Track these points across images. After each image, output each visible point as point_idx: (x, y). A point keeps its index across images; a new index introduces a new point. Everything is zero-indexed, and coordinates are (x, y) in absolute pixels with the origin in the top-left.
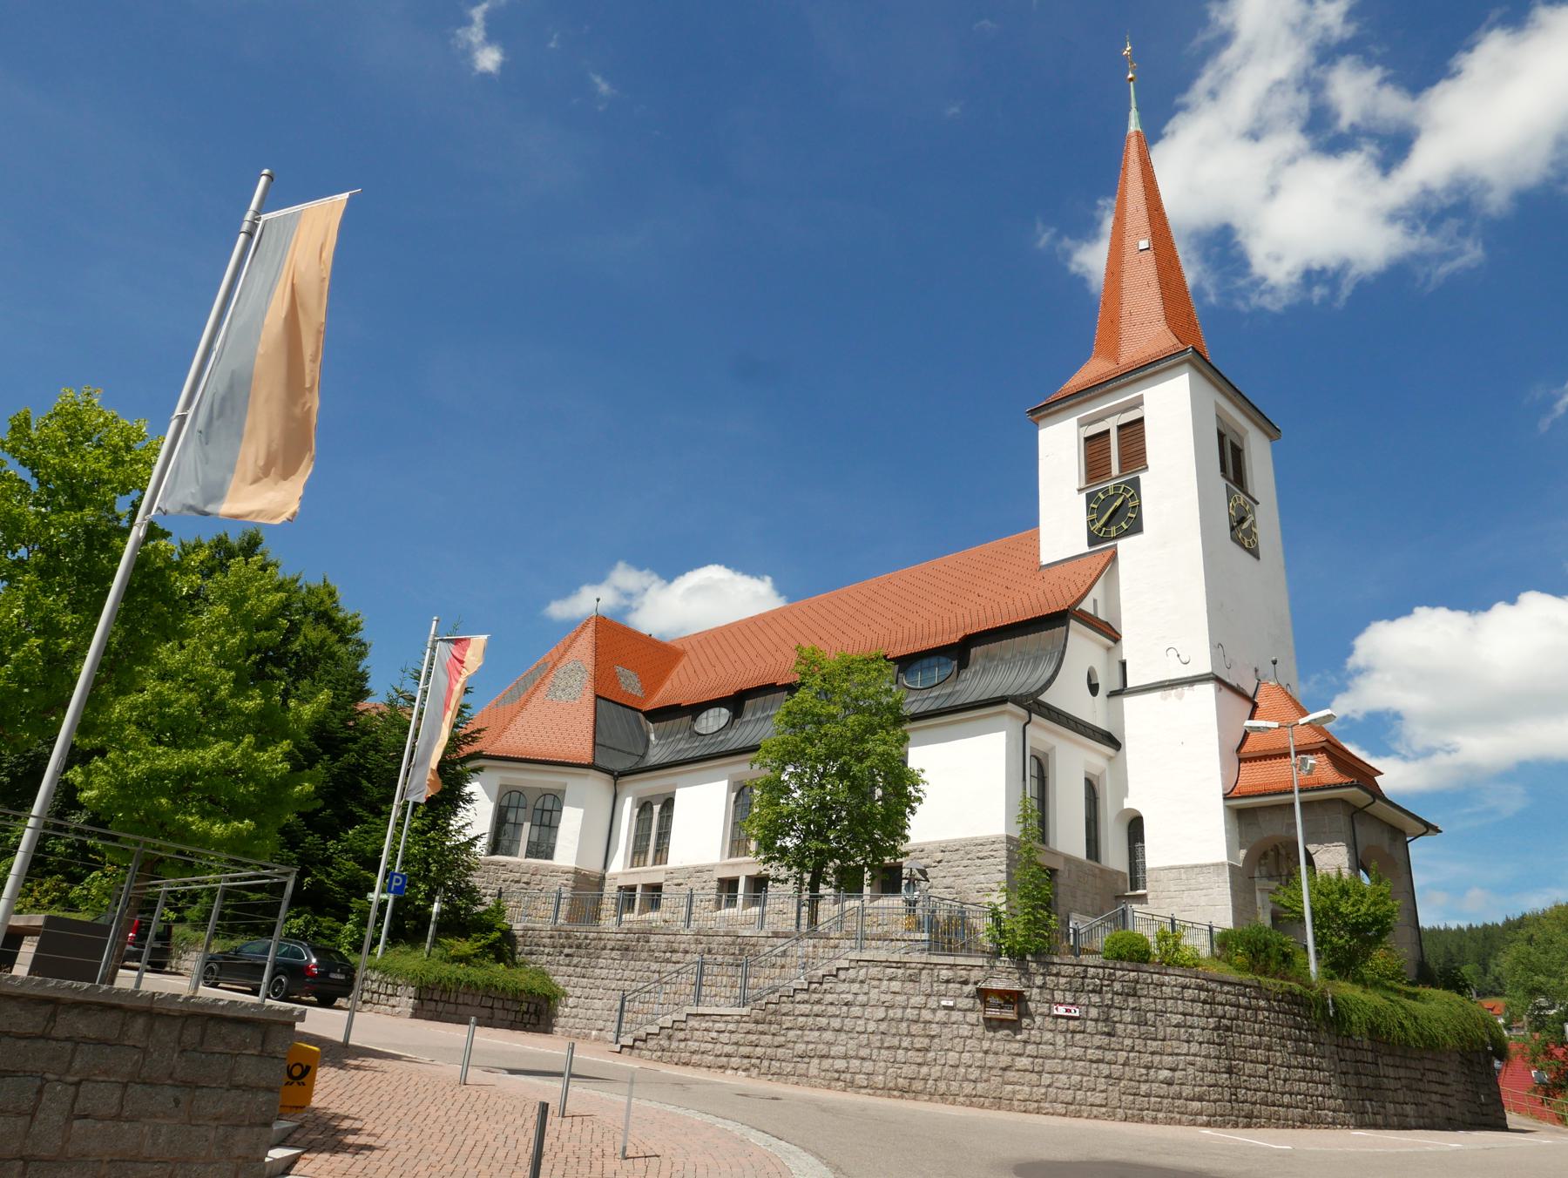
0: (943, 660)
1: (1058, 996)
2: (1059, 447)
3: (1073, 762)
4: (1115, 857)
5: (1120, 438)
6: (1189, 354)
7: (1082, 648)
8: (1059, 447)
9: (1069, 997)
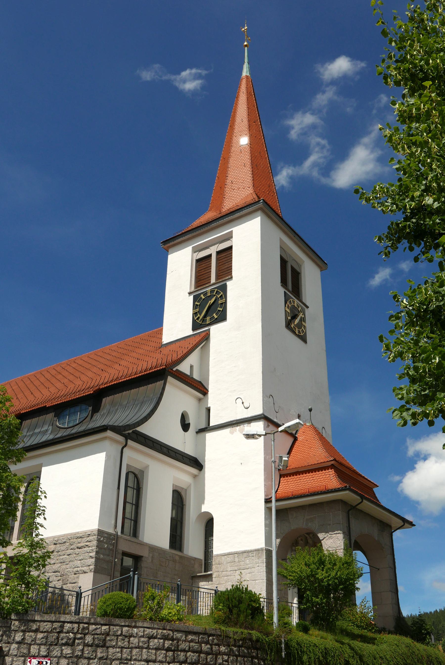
0: (84, 407)
1: (34, 650)
2: (180, 265)
3: (162, 479)
4: (193, 547)
5: (217, 260)
6: (261, 205)
7: (176, 398)
8: (180, 265)
9: (43, 651)
